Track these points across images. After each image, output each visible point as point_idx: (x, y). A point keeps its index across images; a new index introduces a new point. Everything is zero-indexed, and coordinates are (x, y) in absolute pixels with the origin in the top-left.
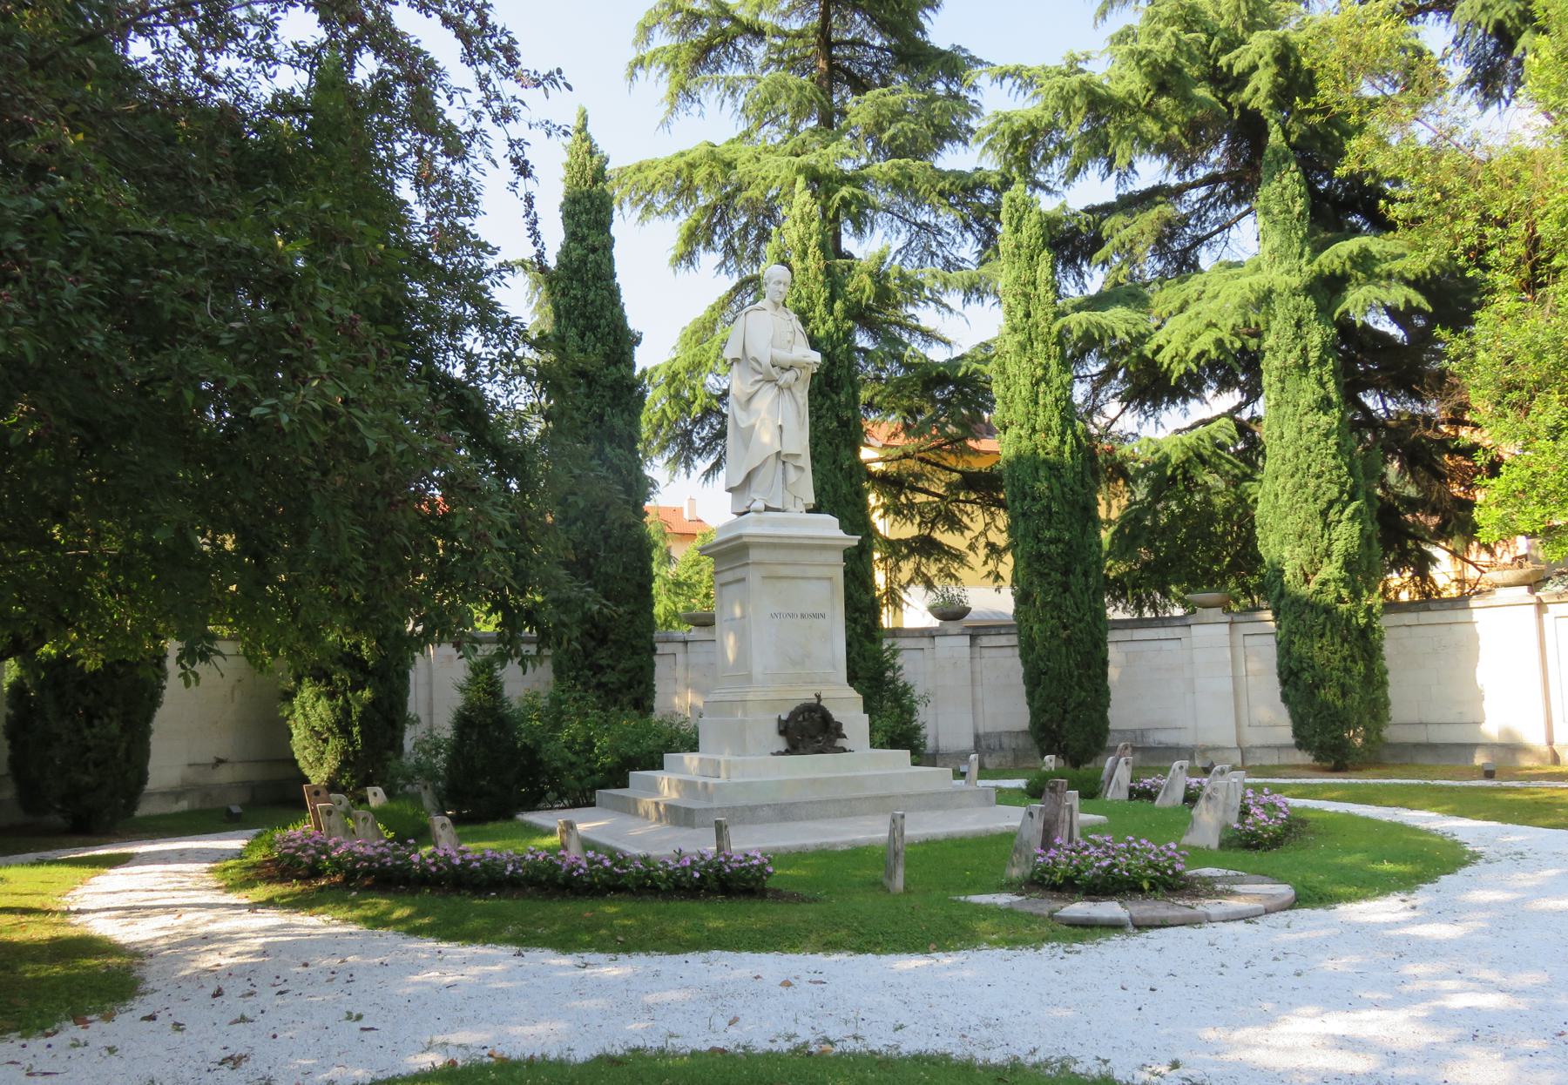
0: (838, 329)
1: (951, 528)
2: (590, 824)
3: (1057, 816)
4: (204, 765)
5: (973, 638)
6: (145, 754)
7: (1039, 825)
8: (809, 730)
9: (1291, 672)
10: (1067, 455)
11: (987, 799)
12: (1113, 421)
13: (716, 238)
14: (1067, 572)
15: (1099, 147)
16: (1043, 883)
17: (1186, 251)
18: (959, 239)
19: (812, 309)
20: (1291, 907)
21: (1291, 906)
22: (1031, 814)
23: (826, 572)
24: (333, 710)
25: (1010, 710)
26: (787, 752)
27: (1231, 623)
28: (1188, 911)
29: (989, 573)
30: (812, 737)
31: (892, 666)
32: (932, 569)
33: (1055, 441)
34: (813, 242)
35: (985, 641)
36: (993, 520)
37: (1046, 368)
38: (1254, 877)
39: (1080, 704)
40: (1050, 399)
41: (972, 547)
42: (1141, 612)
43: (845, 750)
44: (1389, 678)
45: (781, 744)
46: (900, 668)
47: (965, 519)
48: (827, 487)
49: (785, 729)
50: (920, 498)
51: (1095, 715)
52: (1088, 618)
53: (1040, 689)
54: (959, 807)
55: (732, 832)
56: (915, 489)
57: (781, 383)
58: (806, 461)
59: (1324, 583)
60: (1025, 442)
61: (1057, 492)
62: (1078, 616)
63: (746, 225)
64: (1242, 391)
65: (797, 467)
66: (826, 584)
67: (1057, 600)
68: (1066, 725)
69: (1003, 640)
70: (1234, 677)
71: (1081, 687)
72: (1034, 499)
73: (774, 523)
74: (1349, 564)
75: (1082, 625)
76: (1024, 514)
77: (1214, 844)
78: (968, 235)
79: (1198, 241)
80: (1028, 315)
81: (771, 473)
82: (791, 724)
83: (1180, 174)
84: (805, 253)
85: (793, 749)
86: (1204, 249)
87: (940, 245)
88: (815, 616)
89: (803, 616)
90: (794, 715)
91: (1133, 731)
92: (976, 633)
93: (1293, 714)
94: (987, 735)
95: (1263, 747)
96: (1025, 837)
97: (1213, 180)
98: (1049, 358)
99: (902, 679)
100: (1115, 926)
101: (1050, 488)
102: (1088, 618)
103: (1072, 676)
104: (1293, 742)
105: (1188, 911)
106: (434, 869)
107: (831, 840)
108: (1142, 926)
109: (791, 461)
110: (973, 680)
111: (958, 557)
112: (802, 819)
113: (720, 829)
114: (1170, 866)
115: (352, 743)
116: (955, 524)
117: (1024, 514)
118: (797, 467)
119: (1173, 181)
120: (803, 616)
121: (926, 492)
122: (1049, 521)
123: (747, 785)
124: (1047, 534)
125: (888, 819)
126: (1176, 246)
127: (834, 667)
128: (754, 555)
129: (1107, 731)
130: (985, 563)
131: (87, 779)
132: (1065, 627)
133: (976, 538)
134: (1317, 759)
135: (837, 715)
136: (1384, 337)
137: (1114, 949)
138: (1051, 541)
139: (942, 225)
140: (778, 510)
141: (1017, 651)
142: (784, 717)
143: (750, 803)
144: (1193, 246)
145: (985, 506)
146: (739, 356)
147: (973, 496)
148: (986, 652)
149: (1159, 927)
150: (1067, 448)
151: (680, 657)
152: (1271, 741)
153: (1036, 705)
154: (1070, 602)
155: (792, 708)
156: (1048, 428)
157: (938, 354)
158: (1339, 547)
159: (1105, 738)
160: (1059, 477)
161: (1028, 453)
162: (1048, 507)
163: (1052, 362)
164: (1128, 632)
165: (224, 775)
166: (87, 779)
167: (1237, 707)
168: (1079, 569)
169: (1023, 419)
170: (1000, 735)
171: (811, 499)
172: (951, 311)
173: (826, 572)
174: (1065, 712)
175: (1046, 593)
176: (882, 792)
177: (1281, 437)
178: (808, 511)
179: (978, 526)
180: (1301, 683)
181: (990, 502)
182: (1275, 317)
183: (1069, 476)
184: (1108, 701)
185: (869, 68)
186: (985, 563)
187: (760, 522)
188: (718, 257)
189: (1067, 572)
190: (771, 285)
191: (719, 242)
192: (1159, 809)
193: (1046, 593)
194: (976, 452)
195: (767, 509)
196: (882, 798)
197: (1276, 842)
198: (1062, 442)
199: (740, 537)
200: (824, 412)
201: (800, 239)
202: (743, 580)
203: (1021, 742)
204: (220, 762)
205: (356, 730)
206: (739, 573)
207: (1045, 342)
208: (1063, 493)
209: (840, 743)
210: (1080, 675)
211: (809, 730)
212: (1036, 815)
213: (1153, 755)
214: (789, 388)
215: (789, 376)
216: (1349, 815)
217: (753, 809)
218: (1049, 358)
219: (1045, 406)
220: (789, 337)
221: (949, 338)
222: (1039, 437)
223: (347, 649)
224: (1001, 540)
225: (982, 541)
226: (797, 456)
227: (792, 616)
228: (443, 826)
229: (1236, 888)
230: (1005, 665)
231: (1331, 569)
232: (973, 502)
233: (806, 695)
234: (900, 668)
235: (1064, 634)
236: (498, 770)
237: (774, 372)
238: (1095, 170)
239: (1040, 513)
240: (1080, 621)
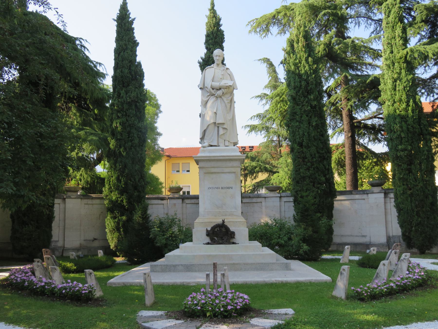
0: (310, 69)
4: (90, 240)
10: (410, 111)
19: (300, 63)
23: (233, 170)
24: (114, 223)
33: (404, 106)
34: (301, 36)
35: (187, 201)
37: (400, 73)
40: (401, 87)
45: (208, 240)
48: (306, 134)
49: (208, 234)
54: (272, 270)
60: (391, 107)
61: (405, 128)
65: (224, 128)
66: (233, 175)
67: (405, 177)
72: (395, 132)
73: (210, 151)
77: (343, 296)
80: (392, 52)
84: (298, 40)
88: (228, 188)
89: (222, 188)
94: (393, 236)
98: (401, 69)
101: (401, 127)
109: (220, 126)
114: (186, 308)
115: (120, 235)
120: (222, 188)
124: (400, 147)
131: (24, 244)
132: (410, 189)
135: (232, 229)
138: (402, 150)
143: (174, 264)
150: (410, 108)
151: (263, 204)
156: (400, 100)
160: (406, 122)
161: (392, 112)
163: (403, 71)
166: (24, 244)
169: (389, 97)
173: (233, 170)
175: (400, 174)
182: (326, 33)
183: (410, 121)
193: (400, 174)
198: (408, 105)
200: (304, 103)
201: (296, 36)
204: (95, 239)
205: (121, 230)
207: (399, 62)
208: (408, 128)
209: (234, 240)
217: (175, 266)
218: (401, 69)
219: (399, 90)
222: (396, 105)
223: (119, 202)
227: (217, 188)
233: (219, 221)
235: (409, 192)
237: (213, 92)
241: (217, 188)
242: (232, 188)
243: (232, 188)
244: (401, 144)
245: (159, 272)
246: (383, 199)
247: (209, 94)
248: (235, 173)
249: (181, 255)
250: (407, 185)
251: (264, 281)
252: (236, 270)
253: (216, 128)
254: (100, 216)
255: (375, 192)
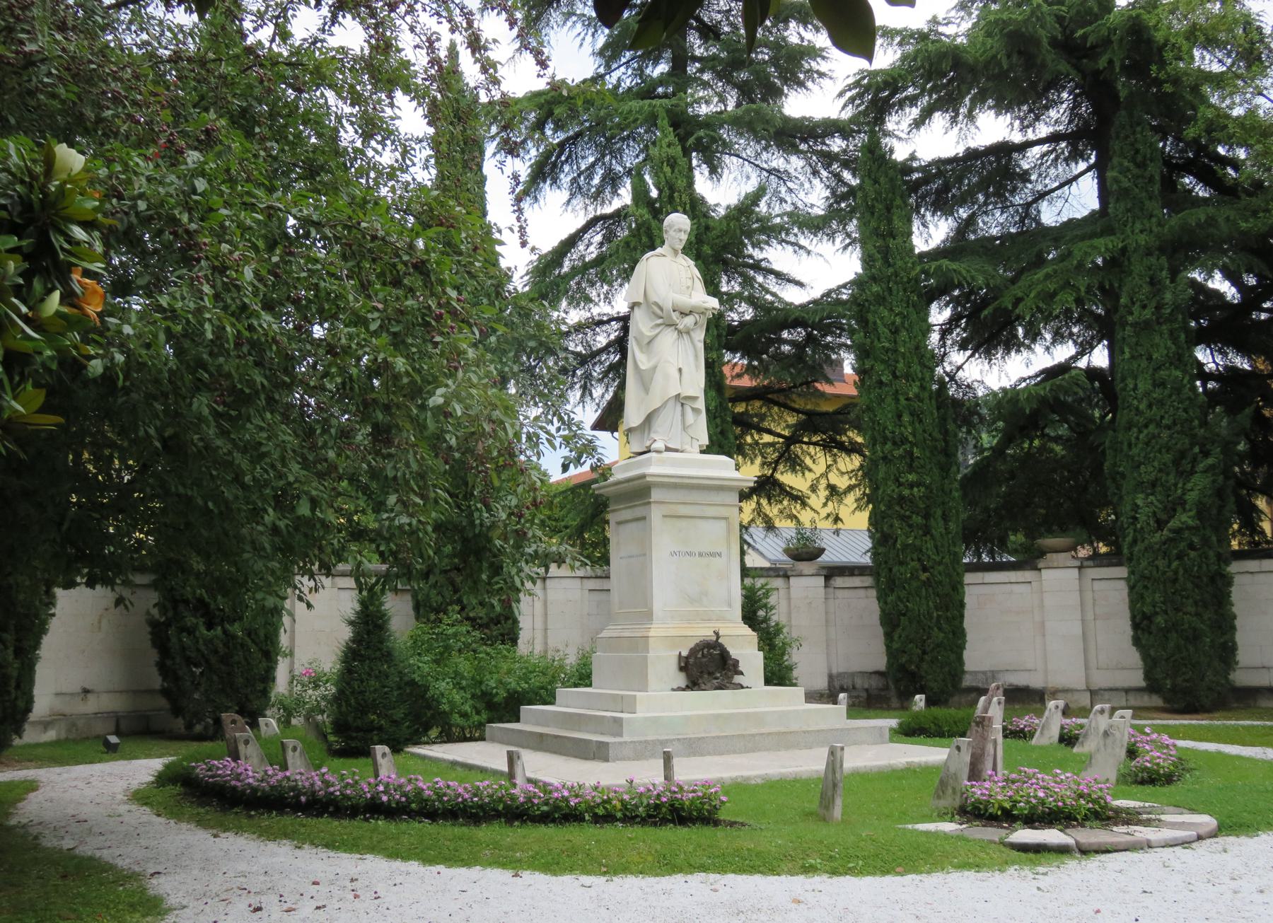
1: (794, 470)
2: (486, 755)
3: (983, 749)
4: (72, 694)
5: (828, 578)
6: (31, 682)
7: (966, 758)
8: (707, 666)
9: (1147, 617)
11: (881, 735)
12: (959, 368)
13: (562, 176)
14: (927, 516)
15: (948, 102)
16: (975, 813)
17: (1028, 206)
18: (807, 185)
20: (1215, 836)
21: (1213, 835)
22: (958, 748)
23: (723, 512)
25: (868, 652)
26: (688, 688)
27: (1080, 568)
28: (1129, 838)
29: (828, 515)
30: (710, 674)
31: (765, 606)
32: (772, 511)
35: (839, 581)
36: (835, 461)
38: (1171, 809)
39: (938, 646)
41: (814, 488)
42: (980, 557)
43: (742, 687)
44: (1237, 623)
45: (681, 680)
46: (772, 608)
47: (808, 461)
49: (685, 665)
50: (767, 438)
51: (953, 657)
52: (947, 560)
53: (899, 630)
55: (677, 762)
56: (761, 430)
57: (681, 327)
58: (701, 404)
59: (1178, 531)
62: (937, 558)
63: (593, 165)
64: (1075, 343)
66: (723, 524)
67: (918, 542)
68: (925, 666)
69: (856, 581)
70: (1083, 621)
71: (940, 629)
73: (674, 463)
74: (1201, 511)
75: (941, 568)
76: (885, 458)
78: (816, 182)
79: (1041, 196)
81: (673, 413)
82: (691, 660)
83: (1023, 129)
85: (693, 685)
86: (1045, 203)
87: (790, 190)
88: (712, 555)
89: (701, 555)
90: (693, 652)
91: (984, 673)
92: (833, 573)
93: (1145, 657)
94: (839, 675)
95: (1111, 690)
96: (952, 770)
97: (1054, 138)
99: (775, 618)
100: (1063, 850)
102: (947, 560)
103: (931, 618)
104: (1143, 684)
105: (1129, 838)
106: (385, 798)
107: (746, 773)
108: (1085, 851)
110: (827, 621)
111: (800, 499)
112: (709, 754)
113: (668, 758)
116: (795, 464)
117: (885, 458)
118: (694, 409)
119: (1017, 138)
120: (701, 555)
121: (770, 432)
122: (910, 466)
123: (655, 720)
125: (825, 752)
126: (1017, 200)
127: (730, 605)
128: (656, 495)
129: (963, 672)
130: (825, 505)
132: (925, 569)
133: (818, 479)
134: (1166, 700)
135: (734, 652)
136: (1218, 295)
137: (1073, 872)
138: (911, 486)
139: (791, 171)
140: (676, 451)
141: (873, 593)
142: (685, 654)
144: (1035, 201)
145: (826, 446)
146: (641, 300)
147: (814, 439)
148: (840, 593)
149: (1108, 851)
152: (1119, 684)
153: (895, 646)
154: (930, 545)
155: (692, 645)
157: (794, 296)
158: (1192, 497)
159: (961, 679)
162: (911, 454)
164: (980, 575)
165: (91, 705)
167: (1085, 650)
168: (939, 512)
170: (853, 675)
171: (706, 441)
172: (809, 252)
173: (723, 512)
174: (924, 653)
176: (783, 729)
177: (1135, 388)
178: (702, 452)
179: (820, 468)
180: (1153, 628)
181: (833, 445)
184: (964, 642)
185: (719, 17)
186: (825, 505)
187: (662, 463)
188: (565, 195)
189: (927, 516)
190: (672, 233)
191: (565, 179)
192: (1034, 748)
194: (822, 395)
195: (668, 449)
196: (779, 734)
197: (1169, 779)
199: (643, 476)
202: (644, 518)
203: (875, 683)
204: (86, 691)
206: (638, 512)
209: (738, 679)
210: (939, 617)
211: (707, 666)
212: (964, 748)
213: (1024, 698)
214: (688, 333)
215: (689, 321)
216: (1219, 753)
220: (690, 283)
221: (803, 280)
224: (842, 483)
225: (823, 482)
226: (694, 398)
227: (690, 554)
228: (384, 755)
229: (1163, 817)
230: (861, 605)
231: (1184, 518)
232: (815, 444)
233: (704, 632)
234: (772, 608)
235: (924, 576)
236: (376, 703)
237: (675, 316)
238: (939, 120)
239: (902, 457)
240: (940, 563)
241: (690, 554)
242: (720, 555)
243: (720, 555)
244: (911, 469)
245: (629, 759)
246: (822, 590)
247: (660, 321)
248: (726, 518)
249: (659, 718)
250: (919, 560)
251: (890, 766)
252: (788, 747)
253: (679, 408)
254: (100, 622)
255: (806, 572)
